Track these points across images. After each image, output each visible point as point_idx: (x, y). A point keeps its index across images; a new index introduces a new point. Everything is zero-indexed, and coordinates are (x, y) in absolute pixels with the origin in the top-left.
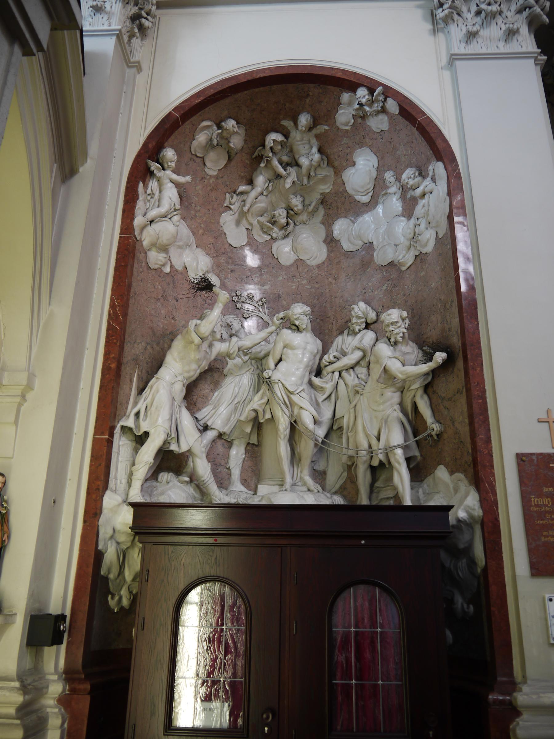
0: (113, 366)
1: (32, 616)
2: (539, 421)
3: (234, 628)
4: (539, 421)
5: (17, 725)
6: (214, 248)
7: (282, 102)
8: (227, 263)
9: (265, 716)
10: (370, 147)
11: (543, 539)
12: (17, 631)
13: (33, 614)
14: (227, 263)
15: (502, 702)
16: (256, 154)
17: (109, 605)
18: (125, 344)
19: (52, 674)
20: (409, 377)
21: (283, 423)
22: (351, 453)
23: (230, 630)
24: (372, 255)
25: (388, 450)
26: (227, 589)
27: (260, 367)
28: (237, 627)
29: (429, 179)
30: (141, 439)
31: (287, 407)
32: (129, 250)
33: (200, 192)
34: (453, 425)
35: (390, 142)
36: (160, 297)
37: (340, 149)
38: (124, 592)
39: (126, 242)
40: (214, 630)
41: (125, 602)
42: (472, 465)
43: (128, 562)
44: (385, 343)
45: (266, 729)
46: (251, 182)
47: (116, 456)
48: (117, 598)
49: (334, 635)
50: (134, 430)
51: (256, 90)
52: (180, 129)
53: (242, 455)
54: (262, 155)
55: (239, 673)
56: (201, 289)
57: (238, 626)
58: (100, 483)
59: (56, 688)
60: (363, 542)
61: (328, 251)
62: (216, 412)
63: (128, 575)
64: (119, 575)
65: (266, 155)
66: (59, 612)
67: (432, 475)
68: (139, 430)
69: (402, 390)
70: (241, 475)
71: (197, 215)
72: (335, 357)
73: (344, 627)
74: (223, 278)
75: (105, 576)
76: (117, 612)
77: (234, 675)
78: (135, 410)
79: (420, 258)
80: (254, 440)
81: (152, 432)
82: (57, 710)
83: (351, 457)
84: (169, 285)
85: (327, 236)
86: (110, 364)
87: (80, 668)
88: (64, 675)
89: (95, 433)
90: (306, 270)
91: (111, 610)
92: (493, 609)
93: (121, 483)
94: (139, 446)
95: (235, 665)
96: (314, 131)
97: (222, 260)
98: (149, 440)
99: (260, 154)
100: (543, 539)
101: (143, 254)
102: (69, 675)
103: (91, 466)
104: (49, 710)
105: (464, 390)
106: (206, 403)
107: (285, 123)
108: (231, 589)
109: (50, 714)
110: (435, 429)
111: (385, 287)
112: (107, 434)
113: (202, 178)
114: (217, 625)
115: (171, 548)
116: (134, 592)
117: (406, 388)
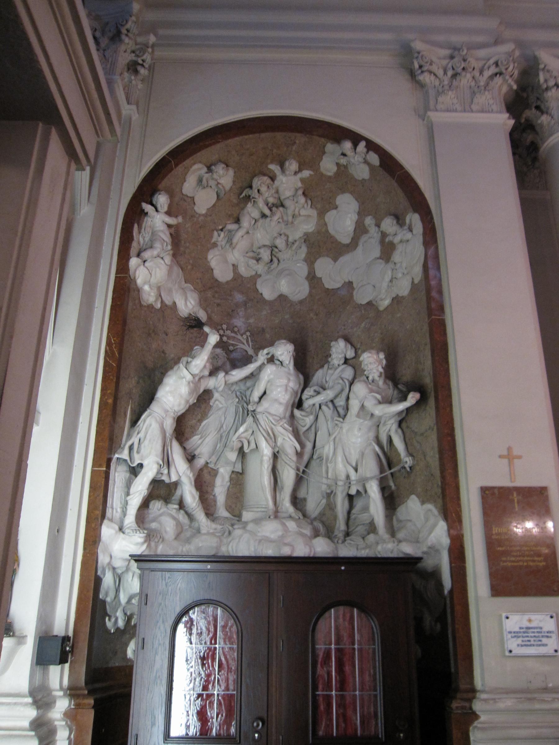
0: (110, 401)
1: (40, 637)
2: (500, 457)
3: (226, 647)
4: (500, 457)
5: (31, 736)
6: (202, 282)
7: (270, 148)
8: (214, 296)
9: (255, 724)
10: (351, 193)
11: (502, 564)
12: (27, 651)
13: (41, 635)
14: (214, 296)
15: (463, 708)
16: (244, 194)
17: (106, 626)
18: (121, 379)
19: (57, 690)
20: (385, 414)
21: (266, 451)
22: (329, 482)
23: (223, 648)
24: (352, 293)
25: (363, 481)
26: (219, 611)
27: (244, 398)
28: (229, 646)
29: (406, 227)
30: (135, 471)
31: (271, 438)
32: (124, 288)
33: (190, 230)
34: (425, 459)
35: (371, 190)
36: (151, 332)
37: (324, 193)
38: (119, 614)
39: (122, 282)
40: (208, 648)
41: (121, 623)
42: (441, 496)
43: (123, 584)
44: (364, 381)
45: (256, 735)
46: (237, 221)
47: (112, 487)
48: (113, 620)
49: (317, 652)
50: (129, 461)
51: (246, 137)
52: (173, 172)
53: (227, 482)
54: (249, 196)
55: (231, 687)
56: (191, 327)
57: (230, 644)
58: (98, 513)
59: (63, 704)
60: (343, 568)
61: (310, 287)
62: (202, 442)
63: (123, 598)
64: (115, 598)
65: (253, 195)
66: (63, 634)
67: (405, 504)
68: (134, 462)
69: (378, 424)
70: (226, 501)
71: (187, 252)
72: (315, 391)
73: (325, 644)
74: (209, 312)
75: (103, 599)
76: (114, 633)
77: (227, 688)
78: (130, 443)
79: (397, 300)
80: (238, 468)
81: (145, 463)
82: (64, 723)
83: (329, 486)
84: (159, 320)
85: (309, 273)
86: (107, 399)
87: (84, 684)
88: (68, 692)
89: (93, 466)
90: (289, 305)
91: (107, 631)
92: (457, 626)
93: (117, 512)
94: (133, 477)
95: (227, 680)
96: (299, 175)
97: (209, 294)
98: (144, 470)
99: (247, 195)
100: (502, 564)
101: (136, 292)
102: (72, 692)
103: (90, 496)
104: (56, 723)
105: (435, 428)
106: (193, 434)
107: (272, 167)
108: (223, 611)
109: (58, 727)
110: (408, 462)
111: (363, 325)
112: (105, 466)
113: (192, 216)
114: (211, 643)
115: (168, 575)
116: (128, 614)
117: (382, 422)
